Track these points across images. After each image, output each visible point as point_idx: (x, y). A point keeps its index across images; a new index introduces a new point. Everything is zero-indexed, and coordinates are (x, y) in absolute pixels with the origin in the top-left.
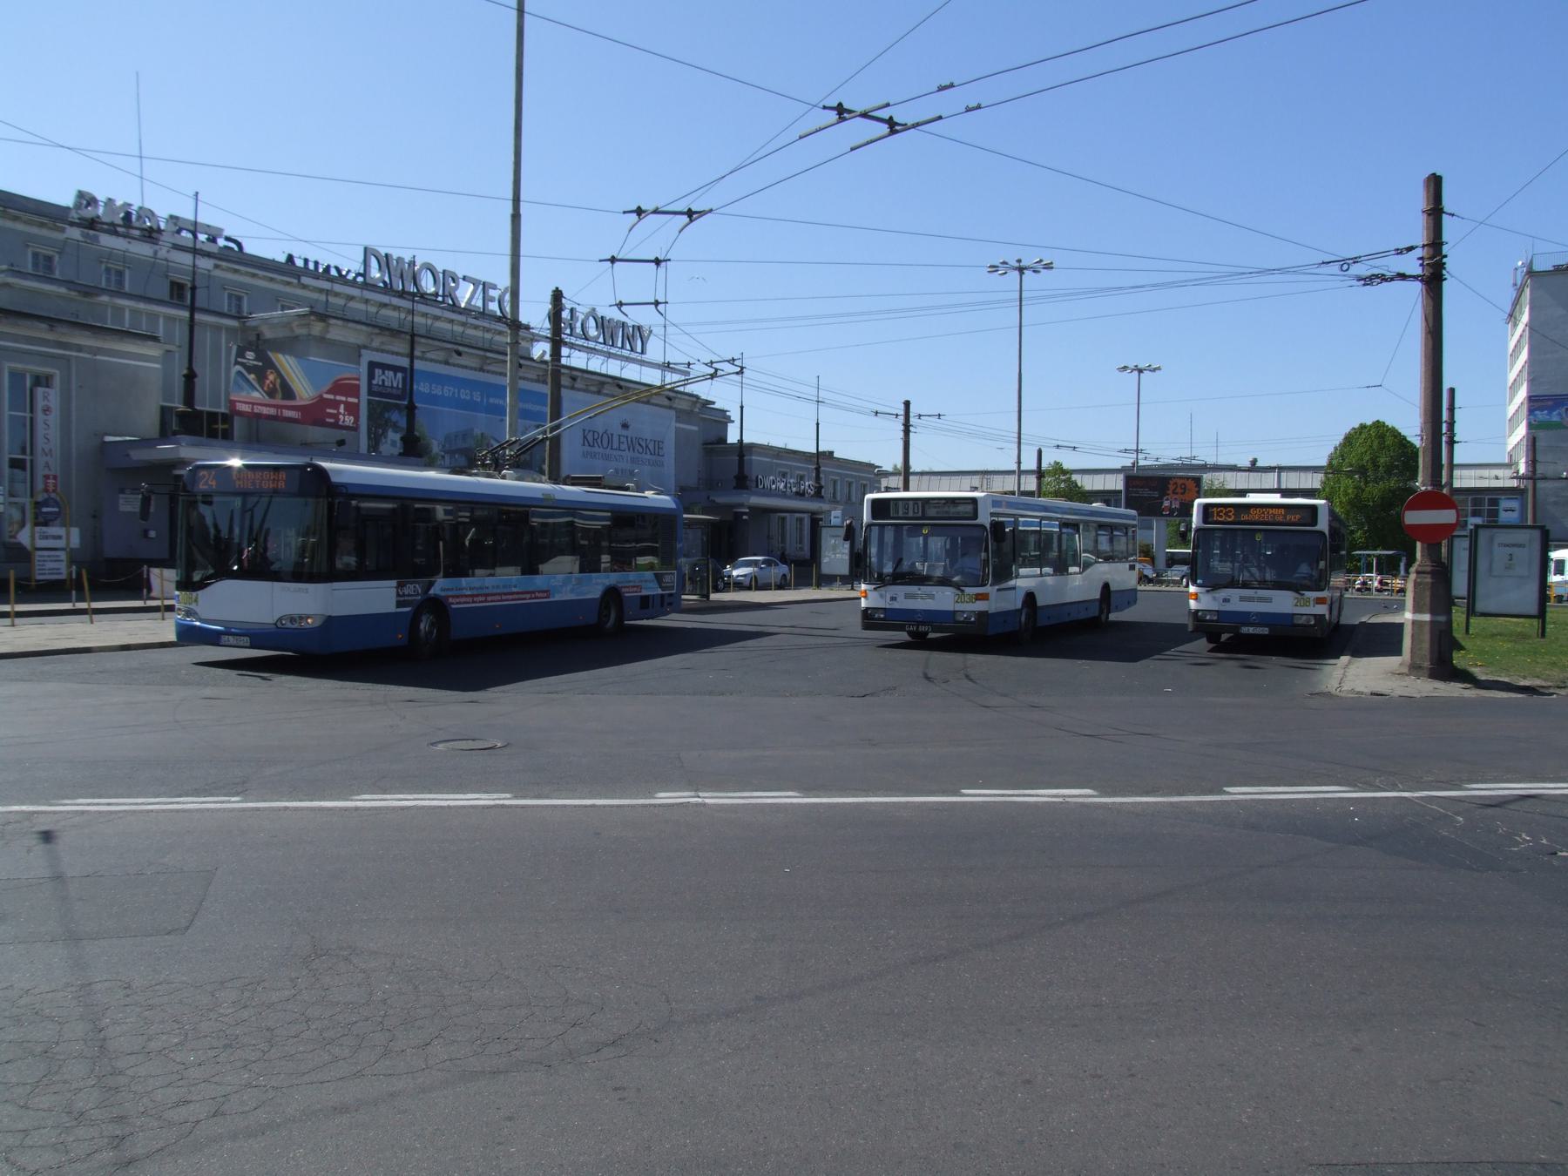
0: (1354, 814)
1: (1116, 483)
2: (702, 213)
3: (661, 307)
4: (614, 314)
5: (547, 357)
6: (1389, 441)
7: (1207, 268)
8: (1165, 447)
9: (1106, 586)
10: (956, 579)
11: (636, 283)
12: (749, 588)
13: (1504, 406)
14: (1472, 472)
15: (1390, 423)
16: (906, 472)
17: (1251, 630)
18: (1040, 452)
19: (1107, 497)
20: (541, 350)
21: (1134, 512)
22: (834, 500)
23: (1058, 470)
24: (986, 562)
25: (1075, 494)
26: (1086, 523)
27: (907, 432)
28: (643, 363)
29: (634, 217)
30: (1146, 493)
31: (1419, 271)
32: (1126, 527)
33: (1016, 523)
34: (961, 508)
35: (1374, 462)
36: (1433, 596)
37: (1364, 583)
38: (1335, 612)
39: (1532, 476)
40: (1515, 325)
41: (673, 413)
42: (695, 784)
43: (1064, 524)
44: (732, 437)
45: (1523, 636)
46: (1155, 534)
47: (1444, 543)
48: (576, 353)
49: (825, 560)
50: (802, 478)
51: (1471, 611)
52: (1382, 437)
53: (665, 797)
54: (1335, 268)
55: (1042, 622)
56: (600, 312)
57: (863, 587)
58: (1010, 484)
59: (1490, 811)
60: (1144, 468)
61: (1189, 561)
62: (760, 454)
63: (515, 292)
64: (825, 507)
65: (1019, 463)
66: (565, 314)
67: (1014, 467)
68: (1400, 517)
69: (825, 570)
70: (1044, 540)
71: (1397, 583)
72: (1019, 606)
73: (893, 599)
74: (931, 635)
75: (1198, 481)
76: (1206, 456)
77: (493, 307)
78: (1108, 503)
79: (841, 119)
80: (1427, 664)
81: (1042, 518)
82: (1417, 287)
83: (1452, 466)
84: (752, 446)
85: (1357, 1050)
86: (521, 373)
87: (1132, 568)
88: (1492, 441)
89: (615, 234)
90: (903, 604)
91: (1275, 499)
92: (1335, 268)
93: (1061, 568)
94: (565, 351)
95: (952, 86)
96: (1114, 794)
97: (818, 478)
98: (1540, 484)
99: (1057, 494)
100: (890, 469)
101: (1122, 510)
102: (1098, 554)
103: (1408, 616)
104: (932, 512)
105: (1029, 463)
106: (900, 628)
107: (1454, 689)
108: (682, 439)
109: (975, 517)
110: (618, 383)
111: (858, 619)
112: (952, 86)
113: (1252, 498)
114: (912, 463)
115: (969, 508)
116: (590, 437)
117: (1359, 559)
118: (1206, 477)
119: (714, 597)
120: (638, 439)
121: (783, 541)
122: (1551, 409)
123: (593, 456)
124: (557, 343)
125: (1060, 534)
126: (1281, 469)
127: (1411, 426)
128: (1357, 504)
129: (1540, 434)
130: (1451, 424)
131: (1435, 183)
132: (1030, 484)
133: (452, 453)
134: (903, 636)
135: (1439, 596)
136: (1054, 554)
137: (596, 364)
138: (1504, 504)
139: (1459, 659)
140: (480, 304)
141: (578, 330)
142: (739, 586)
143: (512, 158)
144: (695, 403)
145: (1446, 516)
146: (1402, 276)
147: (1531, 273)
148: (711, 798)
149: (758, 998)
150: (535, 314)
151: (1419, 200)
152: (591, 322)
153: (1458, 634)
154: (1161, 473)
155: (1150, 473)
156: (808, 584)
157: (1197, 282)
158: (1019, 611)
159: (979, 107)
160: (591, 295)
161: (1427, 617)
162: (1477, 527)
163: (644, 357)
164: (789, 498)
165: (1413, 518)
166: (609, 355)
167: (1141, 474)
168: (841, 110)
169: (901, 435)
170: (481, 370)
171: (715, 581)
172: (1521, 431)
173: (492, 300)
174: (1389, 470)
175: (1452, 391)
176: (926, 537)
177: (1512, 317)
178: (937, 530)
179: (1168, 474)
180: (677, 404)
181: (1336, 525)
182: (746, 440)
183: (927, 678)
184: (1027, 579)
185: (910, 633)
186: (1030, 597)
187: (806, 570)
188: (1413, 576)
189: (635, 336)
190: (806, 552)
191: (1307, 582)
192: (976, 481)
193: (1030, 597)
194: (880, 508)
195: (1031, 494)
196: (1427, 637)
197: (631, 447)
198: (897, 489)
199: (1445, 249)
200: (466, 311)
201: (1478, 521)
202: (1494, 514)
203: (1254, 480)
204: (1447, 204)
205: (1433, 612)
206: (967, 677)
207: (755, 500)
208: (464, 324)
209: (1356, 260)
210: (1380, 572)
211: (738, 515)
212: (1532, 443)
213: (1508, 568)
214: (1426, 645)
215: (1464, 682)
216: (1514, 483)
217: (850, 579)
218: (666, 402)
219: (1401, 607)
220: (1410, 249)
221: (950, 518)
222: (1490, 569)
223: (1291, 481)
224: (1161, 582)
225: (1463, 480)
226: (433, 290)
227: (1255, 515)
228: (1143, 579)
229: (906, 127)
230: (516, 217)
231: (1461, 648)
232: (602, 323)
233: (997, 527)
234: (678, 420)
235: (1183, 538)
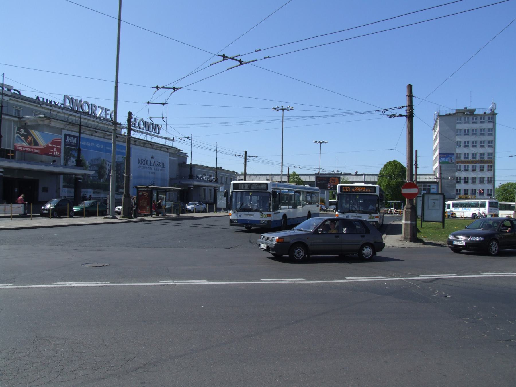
16: (245, 174)
18: (289, 168)
24: (270, 205)
33: (280, 192)
34: (262, 186)
57: (230, 212)
58: (279, 179)
65: (282, 172)
67: (280, 173)
72: (281, 218)
73: (240, 216)
81: (289, 190)
90: (243, 218)
100: (240, 173)
104: (253, 188)
105: (285, 172)
109: (267, 189)
111: (228, 223)
115: (265, 186)
132: (285, 179)
134: (243, 228)
158: (281, 220)
176: (251, 196)
178: (254, 193)
183: (251, 242)
184: (284, 210)
185: (246, 227)
186: (285, 216)
192: (268, 177)
193: (285, 216)
194: (236, 186)
198: (242, 180)
233: (274, 193)
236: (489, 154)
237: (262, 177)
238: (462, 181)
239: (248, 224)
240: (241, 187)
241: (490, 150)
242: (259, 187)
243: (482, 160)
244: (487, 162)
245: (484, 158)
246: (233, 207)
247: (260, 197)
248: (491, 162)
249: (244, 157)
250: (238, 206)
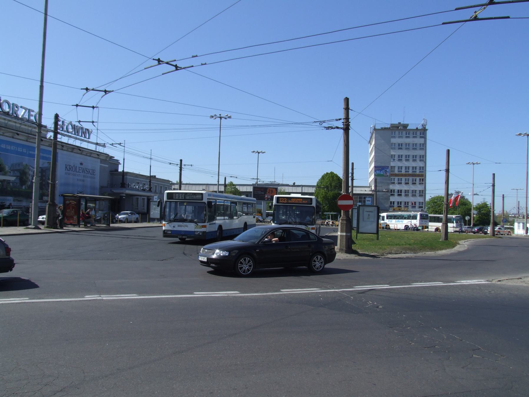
0: (320, 297)
1: (250, 189)
2: (110, 92)
3: (94, 123)
4: (77, 124)
5: (52, 138)
6: (335, 178)
7: (275, 121)
8: (266, 179)
9: (246, 223)
10: (195, 220)
11: (84, 116)
12: (124, 222)
13: (368, 169)
14: (359, 189)
15: (335, 173)
16: (180, 183)
18: (225, 178)
19: (247, 194)
20: (50, 135)
21: (255, 199)
22: (155, 192)
23: (231, 184)
24: (206, 215)
25: (237, 192)
26: (240, 202)
27: (181, 170)
28: (89, 142)
29: (85, 91)
30: (260, 193)
31: (342, 126)
32: (252, 204)
33: (216, 202)
34: (197, 196)
35: (331, 184)
36: (346, 227)
37: (327, 223)
38: (318, 232)
39: (376, 190)
40: (371, 144)
41: (99, 160)
42: (100, 292)
43: (232, 202)
44: (120, 169)
45: (373, 240)
46: (263, 206)
47: (350, 210)
48: (63, 137)
49: (151, 213)
50: (144, 184)
51: (358, 232)
52: (333, 177)
53: (88, 297)
54: (318, 124)
56: (73, 123)
57: (164, 222)
58: (215, 188)
59: (361, 295)
60: (260, 184)
61: (273, 215)
62: (130, 176)
63: (40, 114)
64: (152, 195)
66: (60, 123)
67: (217, 183)
68: (336, 203)
69: (152, 216)
70: (226, 208)
71: (337, 223)
72: (216, 230)
73: (174, 227)
74: (187, 239)
75: (276, 189)
76: (279, 181)
77: (32, 118)
78: (247, 196)
79: (159, 64)
80: (344, 249)
81: (225, 200)
82: (342, 131)
83: (353, 187)
84: (127, 173)
85: (318, 374)
86: (42, 143)
87: (254, 217)
88: (364, 180)
89: (78, 97)
90: (177, 228)
91: (299, 196)
92: (318, 124)
93: (231, 217)
94: (59, 136)
95: (197, 56)
96: (243, 293)
97: (150, 185)
98: (378, 193)
99: (231, 192)
100: (175, 182)
101: (252, 198)
102: (243, 212)
103: (339, 233)
104: (188, 198)
105: (222, 182)
106: (176, 237)
107: (352, 257)
108: (102, 169)
109: (202, 199)
110: (79, 148)
111: (162, 234)
112: (197, 56)
113: (292, 195)
114: (182, 180)
115: (200, 196)
116: (68, 167)
117: (326, 215)
118: (279, 188)
119: (112, 225)
120: (86, 169)
121: (137, 206)
122: (381, 170)
123: (69, 174)
124: (56, 133)
125: (231, 206)
126: (302, 186)
127: (341, 174)
128: (325, 198)
129: (378, 178)
130: (352, 174)
131: (347, 100)
132: (222, 189)
133: (14, 171)
134: (177, 240)
135: (348, 227)
136: (229, 212)
137: (71, 141)
138: (367, 199)
139: (354, 247)
140: (27, 117)
141: (65, 129)
142: (121, 221)
143: (41, 65)
144: (107, 157)
145: (350, 202)
146: (338, 128)
147: (375, 129)
148: (105, 297)
149: (118, 369)
150: (48, 121)
151: (343, 105)
152: (70, 127)
153: (354, 239)
154: (265, 186)
155: (261, 186)
156: (146, 221)
157: (275, 126)
158: (217, 231)
159: (205, 64)
160: (69, 117)
161: (344, 234)
162: (359, 206)
163: (89, 140)
164: (140, 191)
165: (341, 203)
166: (76, 139)
167: (259, 186)
168: (159, 61)
169: (179, 171)
170: (27, 141)
171: (112, 220)
172: (373, 177)
173: (32, 116)
174: (335, 187)
175: (353, 164)
176: (186, 206)
177: (370, 142)
178: (189, 203)
179: (267, 187)
180: (101, 157)
181: (318, 204)
182: (125, 171)
183: (184, 254)
184: (219, 220)
185: (180, 239)
186: (220, 227)
187: (145, 216)
188: (340, 221)
189: (87, 132)
190: (146, 210)
191: (309, 223)
192: (204, 187)
193: (220, 227)
194: (170, 196)
196: (344, 240)
197: (83, 171)
198: (177, 189)
199: (350, 120)
200: (22, 119)
201: (360, 204)
202: (364, 201)
203: (294, 189)
204: (350, 107)
205: (346, 232)
207: (128, 192)
208: (21, 124)
209: (324, 122)
210: (332, 219)
211: (122, 197)
212: (376, 180)
213: (368, 218)
214: (344, 243)
215: (355, 254)
216: (371, 192)
217: (160, 219)
218: (97, 156)
219: (336, 231)
220: (340, 119)
221: (193, 200)
222: (363, 220)
223: (306, 190)
224: (264, 222)
225: (356, 191)
226: (8, 110)
227: (293, 201)
228: (258, 221)
229: (181, 68)
230: (42, 87)
231: (355, 243)
232: (74, 127)
233: (209, 203)
234: (101, 163)
235: (270, 207)
236: (420, 167)
238: (396, 194)
240: (176, 197)
241: (421, 164)
243: (407, 173)
244: (419, 176)
245: (416, 172)
246: (167, 217)
247: (195, 207)
248: (422, 176)
249: (179, 166)
250: (172, 217)
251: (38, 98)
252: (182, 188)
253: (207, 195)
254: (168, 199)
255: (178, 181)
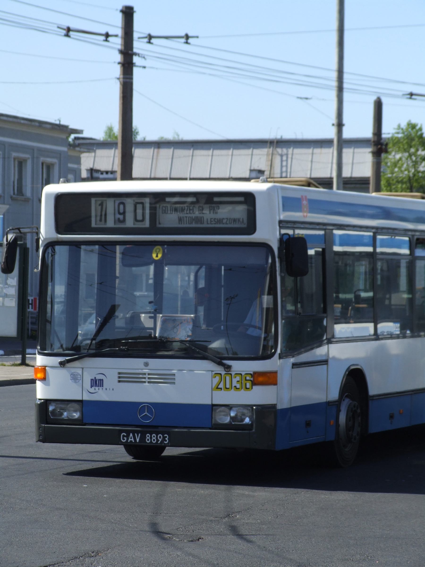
7: (93, 41)
10: (216, 345)
16: (127, 140)
17: (254, 417)
18: (378, 106)
24: (271, 314)
33: (328, 239)
34: (225, 212)
55: (378, 424)
57: (40, 360)
58: (323, 164)
65: (340, 125)
67: (330, 133)
72: (334, 394)
73: (97, 383)
81: (377, 230)
90: (116, 392)
100: (99, 134)
104: (169, 219)
105: (359, 126)
106: (110, 438)
109: (251, 228)
111: (30, 422)
114: (138, 121)
132: (360, 164)
134: (118, 454)
136: (401, 297)
158: (335, 405)
169: (117, 71)
176: (159, 266)
178: (178, 252)
183: (158, 533)
184: (349, 344)
185: (130, 448)
186: (355, 379)
192: (260, 158)
193: (355, 379)
194: (72, 212)
195: (360, 184)
198: (109, 175)
206: (234, 531)
221: (202, 230)
233: (293, 247)
237: (223, 156)
239: (146, 429)
240: (103, 217)
242: (207, 215)
246: (59, 333)
247: (212, 273)
249: (117, 42)
250: (87, 327)
251: (335, 25)
252: (139, 166)
253: (278, 203)
254: (59, 230)
255: (117, 129)
